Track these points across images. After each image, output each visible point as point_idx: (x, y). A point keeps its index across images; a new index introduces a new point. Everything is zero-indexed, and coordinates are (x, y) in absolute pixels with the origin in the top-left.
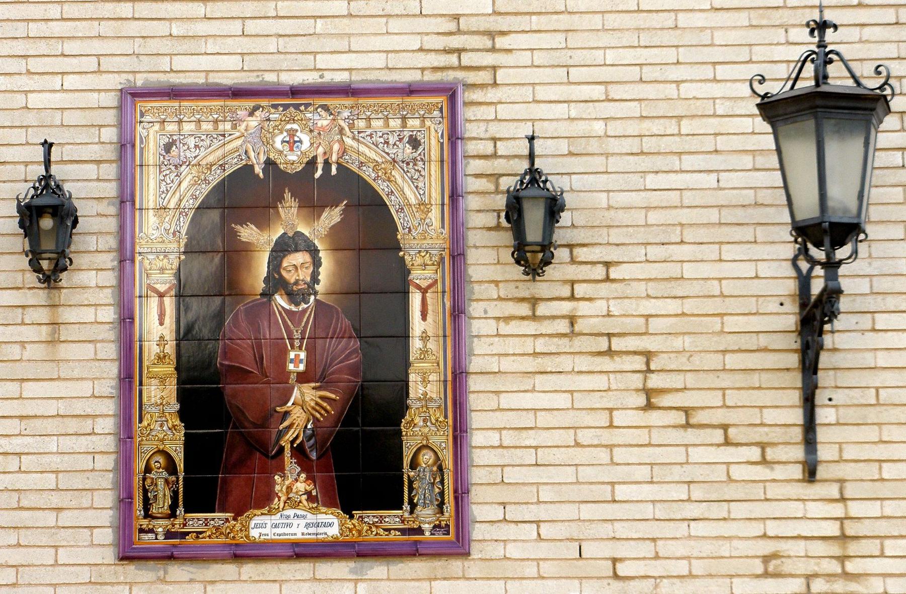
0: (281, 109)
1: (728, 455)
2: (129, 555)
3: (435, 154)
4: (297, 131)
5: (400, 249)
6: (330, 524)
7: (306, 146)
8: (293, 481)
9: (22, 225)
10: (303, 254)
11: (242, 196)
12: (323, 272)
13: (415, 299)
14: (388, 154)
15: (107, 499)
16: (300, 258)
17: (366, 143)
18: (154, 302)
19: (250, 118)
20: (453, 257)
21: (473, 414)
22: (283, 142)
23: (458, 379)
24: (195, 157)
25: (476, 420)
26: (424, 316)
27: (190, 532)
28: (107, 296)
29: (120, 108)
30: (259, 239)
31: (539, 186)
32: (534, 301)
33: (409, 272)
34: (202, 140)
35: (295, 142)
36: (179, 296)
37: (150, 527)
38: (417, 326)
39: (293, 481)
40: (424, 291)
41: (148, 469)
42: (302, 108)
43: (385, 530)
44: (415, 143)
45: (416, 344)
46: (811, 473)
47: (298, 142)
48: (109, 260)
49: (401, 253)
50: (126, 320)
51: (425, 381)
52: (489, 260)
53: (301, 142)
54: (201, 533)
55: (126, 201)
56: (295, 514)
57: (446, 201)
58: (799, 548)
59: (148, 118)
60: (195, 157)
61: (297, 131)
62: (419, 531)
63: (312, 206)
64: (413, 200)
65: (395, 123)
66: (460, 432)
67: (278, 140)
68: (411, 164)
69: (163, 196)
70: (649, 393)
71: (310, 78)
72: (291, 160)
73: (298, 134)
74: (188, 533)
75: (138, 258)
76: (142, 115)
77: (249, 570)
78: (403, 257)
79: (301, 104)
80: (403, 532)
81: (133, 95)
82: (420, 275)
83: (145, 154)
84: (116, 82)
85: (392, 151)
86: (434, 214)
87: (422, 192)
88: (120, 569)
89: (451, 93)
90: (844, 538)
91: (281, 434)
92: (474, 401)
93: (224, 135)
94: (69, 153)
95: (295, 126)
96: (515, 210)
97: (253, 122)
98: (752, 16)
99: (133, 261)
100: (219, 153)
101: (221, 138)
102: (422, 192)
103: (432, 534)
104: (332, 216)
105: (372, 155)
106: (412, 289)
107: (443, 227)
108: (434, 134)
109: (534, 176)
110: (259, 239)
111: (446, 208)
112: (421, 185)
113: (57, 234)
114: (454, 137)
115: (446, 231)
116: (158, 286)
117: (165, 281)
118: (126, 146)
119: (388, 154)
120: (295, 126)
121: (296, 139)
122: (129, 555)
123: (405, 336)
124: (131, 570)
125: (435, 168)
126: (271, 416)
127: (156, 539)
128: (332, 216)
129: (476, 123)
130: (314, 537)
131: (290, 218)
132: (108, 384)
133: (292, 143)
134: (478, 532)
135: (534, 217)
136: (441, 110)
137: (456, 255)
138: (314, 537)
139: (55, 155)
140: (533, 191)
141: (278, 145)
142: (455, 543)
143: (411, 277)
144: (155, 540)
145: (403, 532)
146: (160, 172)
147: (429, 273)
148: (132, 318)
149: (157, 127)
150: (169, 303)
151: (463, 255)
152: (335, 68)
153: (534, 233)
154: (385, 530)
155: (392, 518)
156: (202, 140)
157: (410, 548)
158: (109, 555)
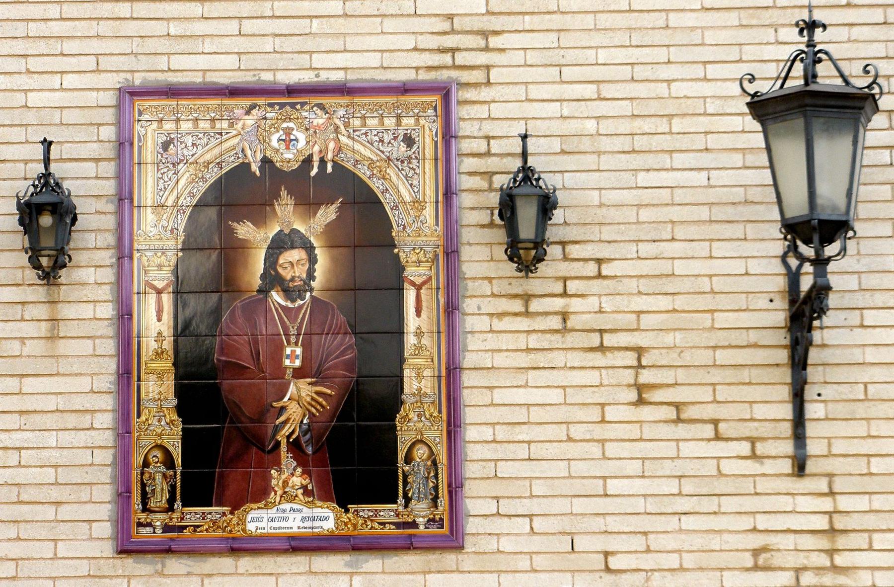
0: (278, 108)
1: (719, 449)
2: (127, 548)
3: (429, 152)
4: (293, 129)
5: (395, 246)
6: (326, 518)
7: (302, 144)
8: (289, 476)
9: (21, 222)
10: (299, 251)
11: (239, 193)
12: (318, 269)
13: (410, 296)
14: (383, 152)
15: (106, 493)
16: (296, 255)
17: (361, 142)
18: (152, 298)
19: (247, 117)
20: (447, 254)
21: (467, 409)
22: (279, 140)
23: (451, 375)
24: (193, 155)
25: (469, 415)
26: (418, 312)
27: (187, 526)
28: (106, 293)
29: (119, 107)
30: (256, 236)
31: (532, 183)
32: (527, 298)
33: (404, 269)
34: (200, 139)
35: (291, 140)
36: (177, 292)
37: (148, 520)
38: (411, 322)
39: (289, 476)
40: (418, 288)
41: (146, 464)
42: (298, 107)
43: (380, 524)
44: (409, 141)
45: (410, 340)
46: (800, 467)
47: (294, 140)
48: (107, 257)
49: (396, 250)
50: (125, 316)
51: (419, 377)
52: (482, 256)
53: (297, 140)
54: (198, 526)
55: (125, 198)
56: (291, 508)
57: (440, 198)
58: (788, 541)
59: (146, 117)
60: (193, 155)
61: (293, 129)
62: (414, 525)
63: (308, 204)
64: (408, 197)
65: (390, 122)
66: (454, 427)
67: (274, 138)
68: (406, 162)
69: (161, 194)
70: (640, 388)
71: (306, 77)
72: (288, 158)
73: (294, 132)
74: (185, 527)
75: (136, 255)
76: (140, 114)
77: (246, 563)
78: (398, 254)
79: (297, 103)
80: (398, 525)
81: (131, 94)
82: (414, 272)
83: (144, 152)
84: (114, 81)
85: (387, 149)
86: (429, 212)
87: (416, 190)
88: (118, 562)
89: (445, 92)
90: (832, 531)
91: (277, 429)
92: (468, 397)
93: (221, 134)
94: (68, 151)
95: (291, 125)
96: (508, 207)
97: (250, 121)
98: (742, 16)
99: (131, 258)
100: (217, 151)
101: (218, 136)
102: (416, 190)
103: (426, 528)
104: (328, 214)
105: (368, 153)
106: (406, 285)
107: (437, 224)
108: (428, 133)
109: (527, 174)
110: (256, 236)
111: (440, 206)
112: (415, 182)
113: (57, 231)
114: (448, 135)
115: (440, 228)
116: (155, 283)
117: (162, 278)
118: (124, 144)
119: (383, 152)
120: (291, 125)
121: (292, 137)
122: (127, 548)
123: (400, 332)
124: (129, 563)
125: (429, 166)
126: (267, 411)
127: (154, 532)
128: (328, 214)
129: (469, 122)
130: (310, 530)
131: (286, 215)
132: (107, 380)
133: (288, 141)
134: (471, 526)
135: (527, 214)
136: (435, 109)
137: (450, 252)
138: (310, 530)
139: (54, 153)
140: (526, 189)
141: (275, 143)
142: (449, 537)
143: (405, 274)
144: (153, 534)
145: (398, 525)
146: (158, 170)
147: (423, 270)
148: (130, 315)
149: (155, 125)
150: (167, 300)
151: (457, 252)
152: (331, 67)
153: (526, 230)
154: (380, 524)
155: (387, 512)
156: (200, 139)
157: (405, 541)
158: (108, 549)
